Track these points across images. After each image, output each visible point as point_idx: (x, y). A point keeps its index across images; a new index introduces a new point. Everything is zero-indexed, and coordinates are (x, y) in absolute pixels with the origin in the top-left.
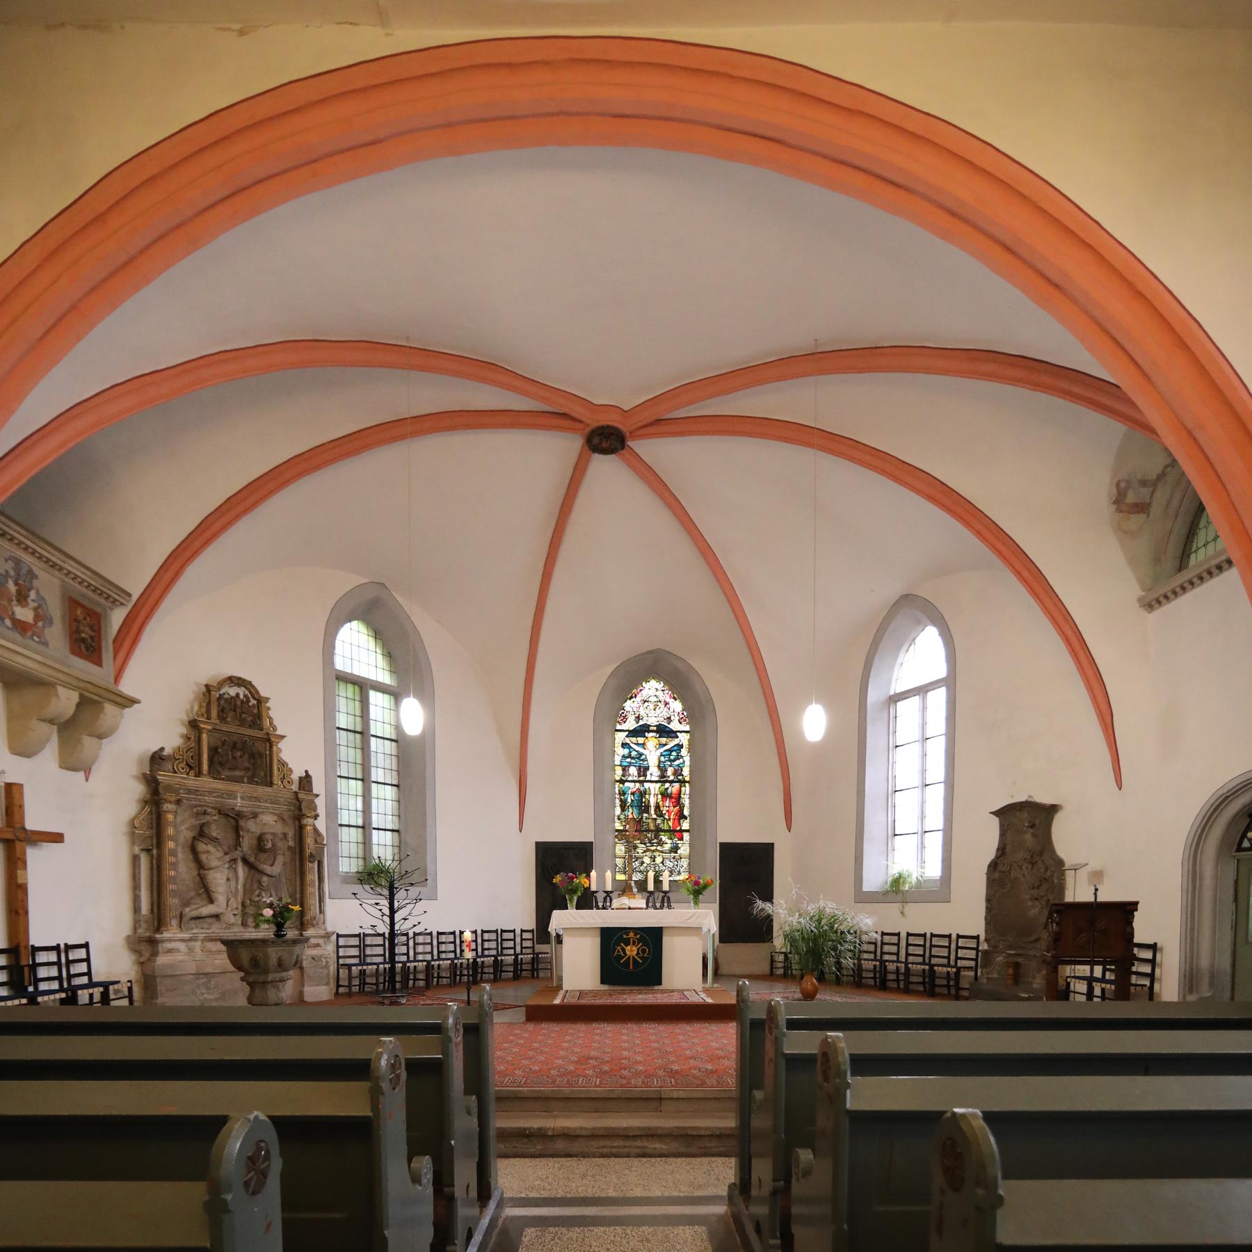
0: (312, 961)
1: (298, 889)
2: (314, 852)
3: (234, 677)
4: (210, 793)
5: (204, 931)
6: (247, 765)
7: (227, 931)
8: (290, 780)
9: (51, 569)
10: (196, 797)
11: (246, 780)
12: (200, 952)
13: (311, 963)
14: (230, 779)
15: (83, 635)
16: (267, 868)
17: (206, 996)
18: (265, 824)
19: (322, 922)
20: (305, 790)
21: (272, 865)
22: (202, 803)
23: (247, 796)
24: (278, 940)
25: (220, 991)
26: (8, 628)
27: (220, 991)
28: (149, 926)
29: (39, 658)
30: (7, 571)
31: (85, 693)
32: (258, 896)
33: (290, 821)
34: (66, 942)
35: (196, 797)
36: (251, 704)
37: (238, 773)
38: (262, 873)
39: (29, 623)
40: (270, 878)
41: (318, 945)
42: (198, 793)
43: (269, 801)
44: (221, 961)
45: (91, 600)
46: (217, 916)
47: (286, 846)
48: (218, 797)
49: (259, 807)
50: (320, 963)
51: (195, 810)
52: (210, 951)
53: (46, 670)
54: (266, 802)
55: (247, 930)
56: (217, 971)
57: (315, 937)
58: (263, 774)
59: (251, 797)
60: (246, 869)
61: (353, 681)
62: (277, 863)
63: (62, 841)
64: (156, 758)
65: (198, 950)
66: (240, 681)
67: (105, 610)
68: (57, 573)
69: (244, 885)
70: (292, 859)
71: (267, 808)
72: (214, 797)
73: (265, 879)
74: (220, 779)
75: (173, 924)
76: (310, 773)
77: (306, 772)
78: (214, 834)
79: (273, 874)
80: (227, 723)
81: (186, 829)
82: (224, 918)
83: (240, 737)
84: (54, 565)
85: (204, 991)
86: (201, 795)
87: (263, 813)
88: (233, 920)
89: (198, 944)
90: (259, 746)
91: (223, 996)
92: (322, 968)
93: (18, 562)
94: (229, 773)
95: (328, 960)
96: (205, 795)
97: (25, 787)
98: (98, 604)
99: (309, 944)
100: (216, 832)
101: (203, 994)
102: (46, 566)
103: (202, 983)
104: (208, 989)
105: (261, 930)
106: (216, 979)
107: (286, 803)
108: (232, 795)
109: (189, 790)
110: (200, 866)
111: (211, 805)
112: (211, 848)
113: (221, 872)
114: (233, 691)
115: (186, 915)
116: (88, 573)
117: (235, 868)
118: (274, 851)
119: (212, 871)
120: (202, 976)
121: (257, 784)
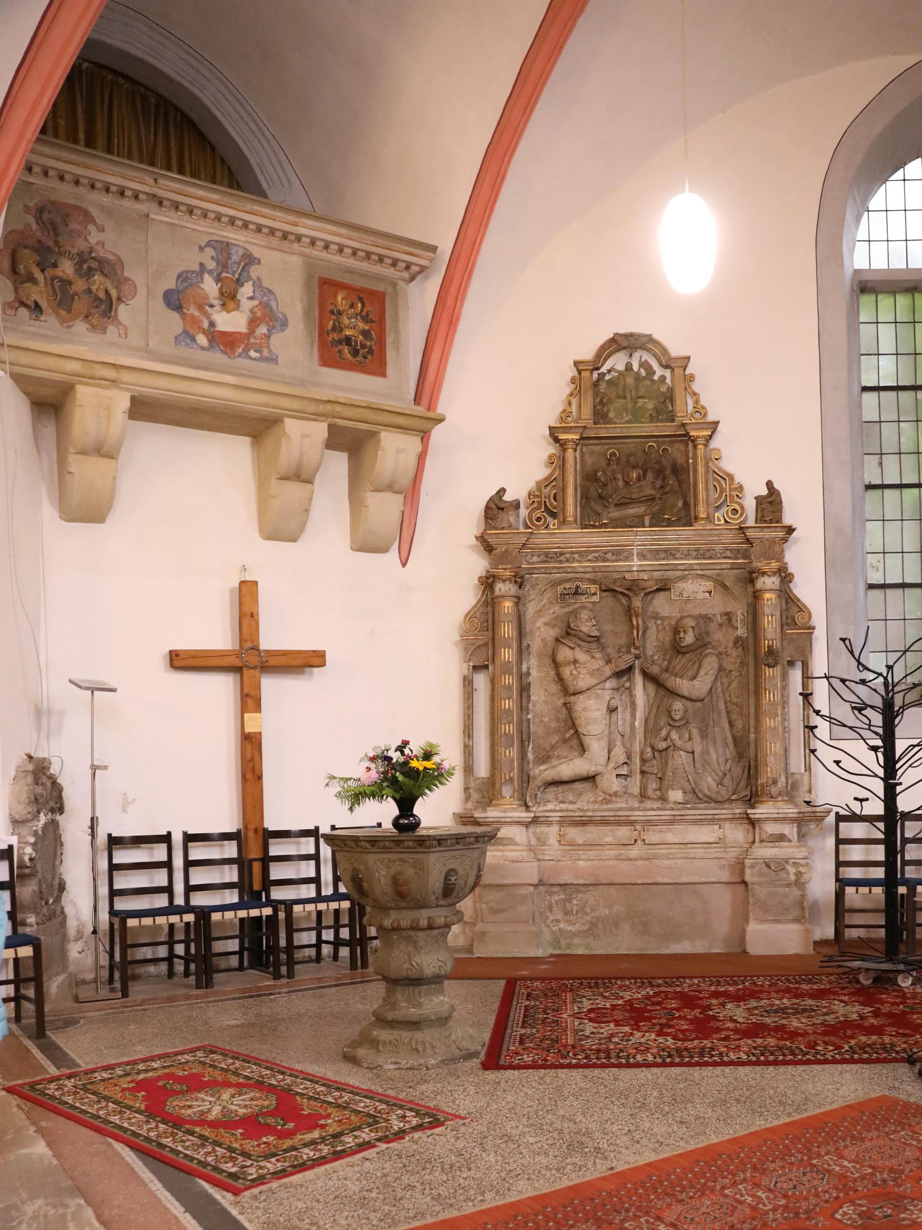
0: (766, 869)
1: (752, 722)
2: (777, 645)
3: (621, 335)
4: (583, 555)
5: (564, 806)
6: (649, 491)
7: (605, 807)
8: (737, 507)
9: (286, 244)
10: (557, 565)
11: (647, 523)
12: (556, 843)
13: (761, 874)
14: (616, 523)
15: (348, 332)
16: (683, 685)
17: (562, 925)
18: (688, 600)
19: (806, 788)
20: (766, 521)
21: (694, 678)
22: (572, 575)
23: (651, 551)
24: (405, 836)
25: (589, 918)
26: (203, 348)
27: (589, 918)
28: (483, 797)
29: (230, 379)
30: (201, 265)
31: (338, 421)
32: (666, 739)
33: (736, 589)
34: (185, 830)
35: (557, 565)
36: (656, 377)
37: (633, 511)
38: (674, 694)
39: (240, 333)
40: (689, 704)
41: (781, 838)
42: (562, 558)
43: (694, 554)
44: (589, 863)
45: (365, 275)
46: (590, 779)
47: (732, 639)
48: (596, 560)
49: (674, 568)
50: (783, 875)
51: (560, 589)
52: (572, 844)
53: (265, 398)
54: (687, 556)
55: (644, 805)
56: (582, 881)
57: (776, 820)
58: (680, 504)
59: (658, 551)
60: (651, 688)
61: (908, 285)
62: (702, 673)
63: (323, 664)
64: (491, 508)
65: (553, 840)
66: (632, 340)
67: (395, 285)
68: (296, 246)
69: (646, 721)
70: (742, 663)
71: (690, 568)
72: (589, 560)
73: (678, 705)
74: (600, 527)
75: (504, 794)
76: (776, 486)
77: (769, 484)
78: (585, 629)
79: (695, 694)
80: (610, 422)
81: (546, 624)
82: (603, 782)
83: (641, 443)
84: (285, 236)
85: (560, 916)
86: (568, 561)
87: (683, 578)
88: (615, 785)
89: (554, 829)
90: (676, 452)
91: (592, 930)
92: (788, 885)
93: (223, 248)
94: (616, 513)
95: (801, 869)
96: (574, 560)
97: (260, 586)
98: (379, 278)
99: (764, 836)
100: (590, 624)
101: (558, 921)
102: (275, 242)
103: (557, 902)
104: (567, 913)
105: (671, 805)
106: (580, 895)
107: (728, 553)
108: (620, 553)
109: (546, 554)
110: (567, 691)
111: (587, 576)
112: (581, 656)
113: (597, 696)
114: (618, 362)
115: (535, 778)
116: (343, 231)
117: (629, 688)
118: (702, 645)
119: (581, 697)
120: (556, 889)
121: (670, 523)
